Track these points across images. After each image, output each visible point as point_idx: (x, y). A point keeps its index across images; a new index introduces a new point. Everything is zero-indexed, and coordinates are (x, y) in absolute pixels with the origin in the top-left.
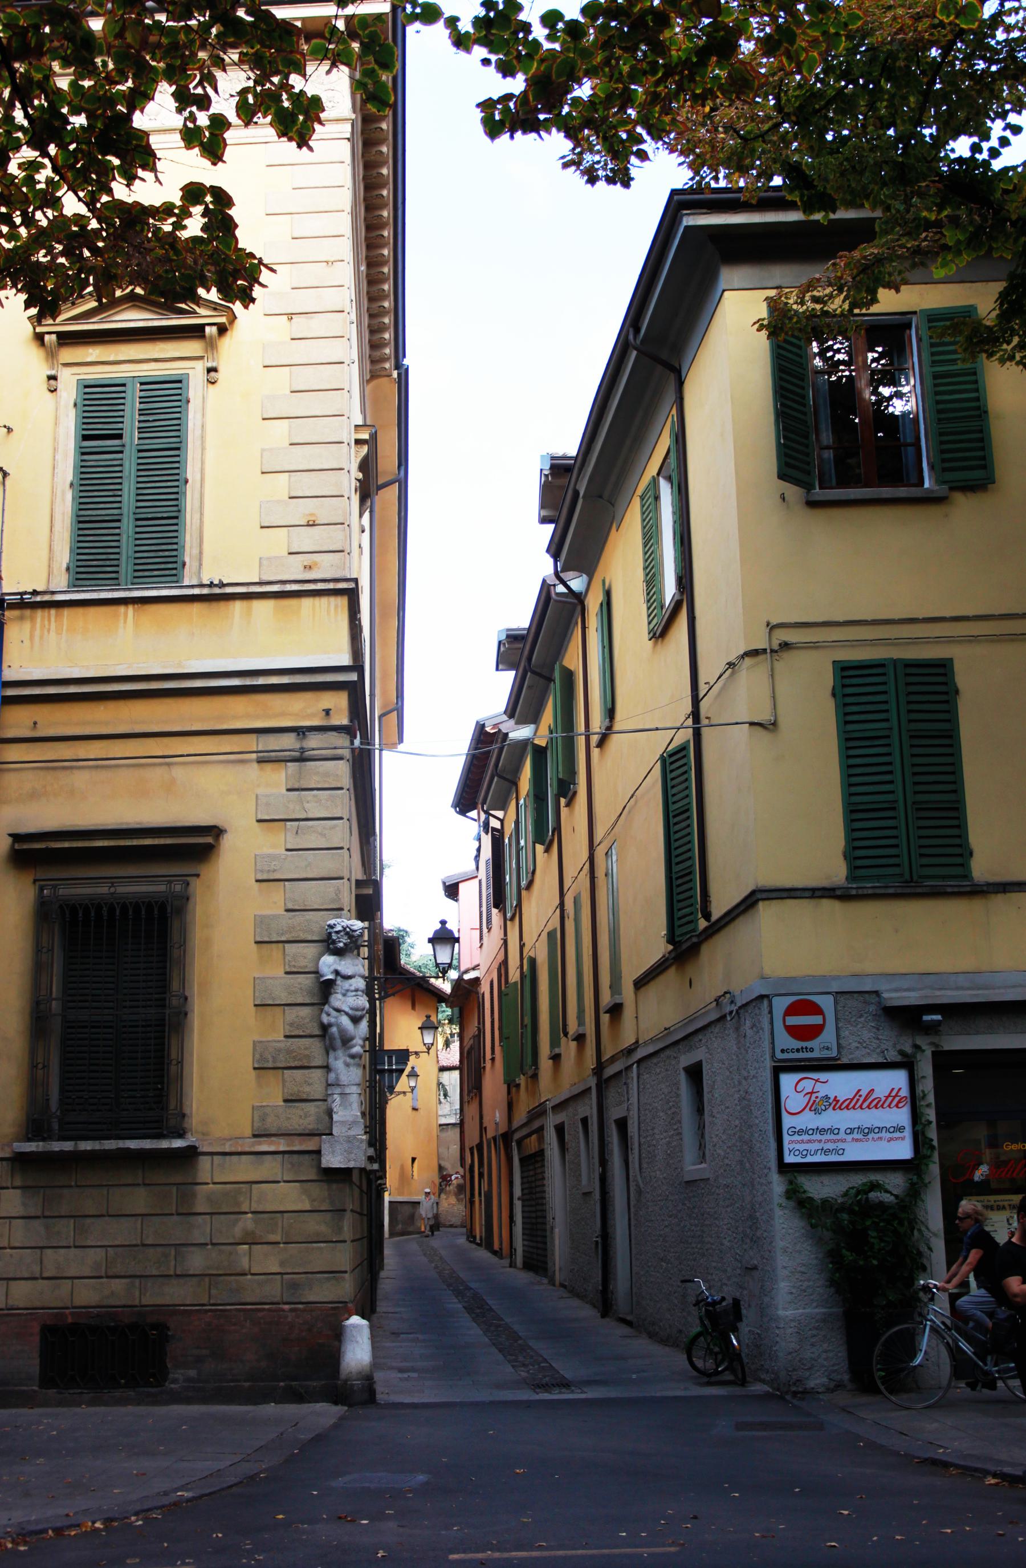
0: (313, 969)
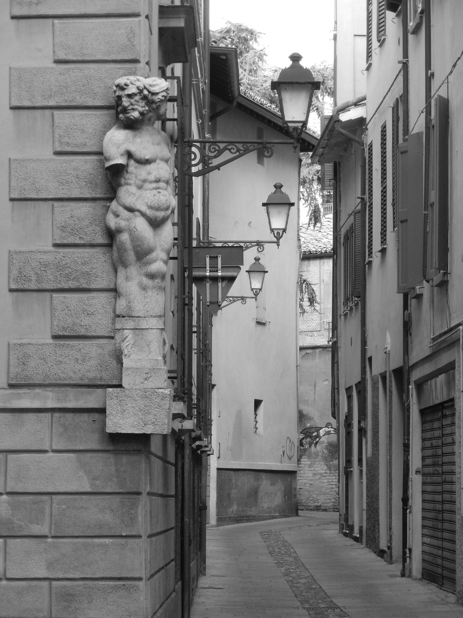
0: (94, 149)
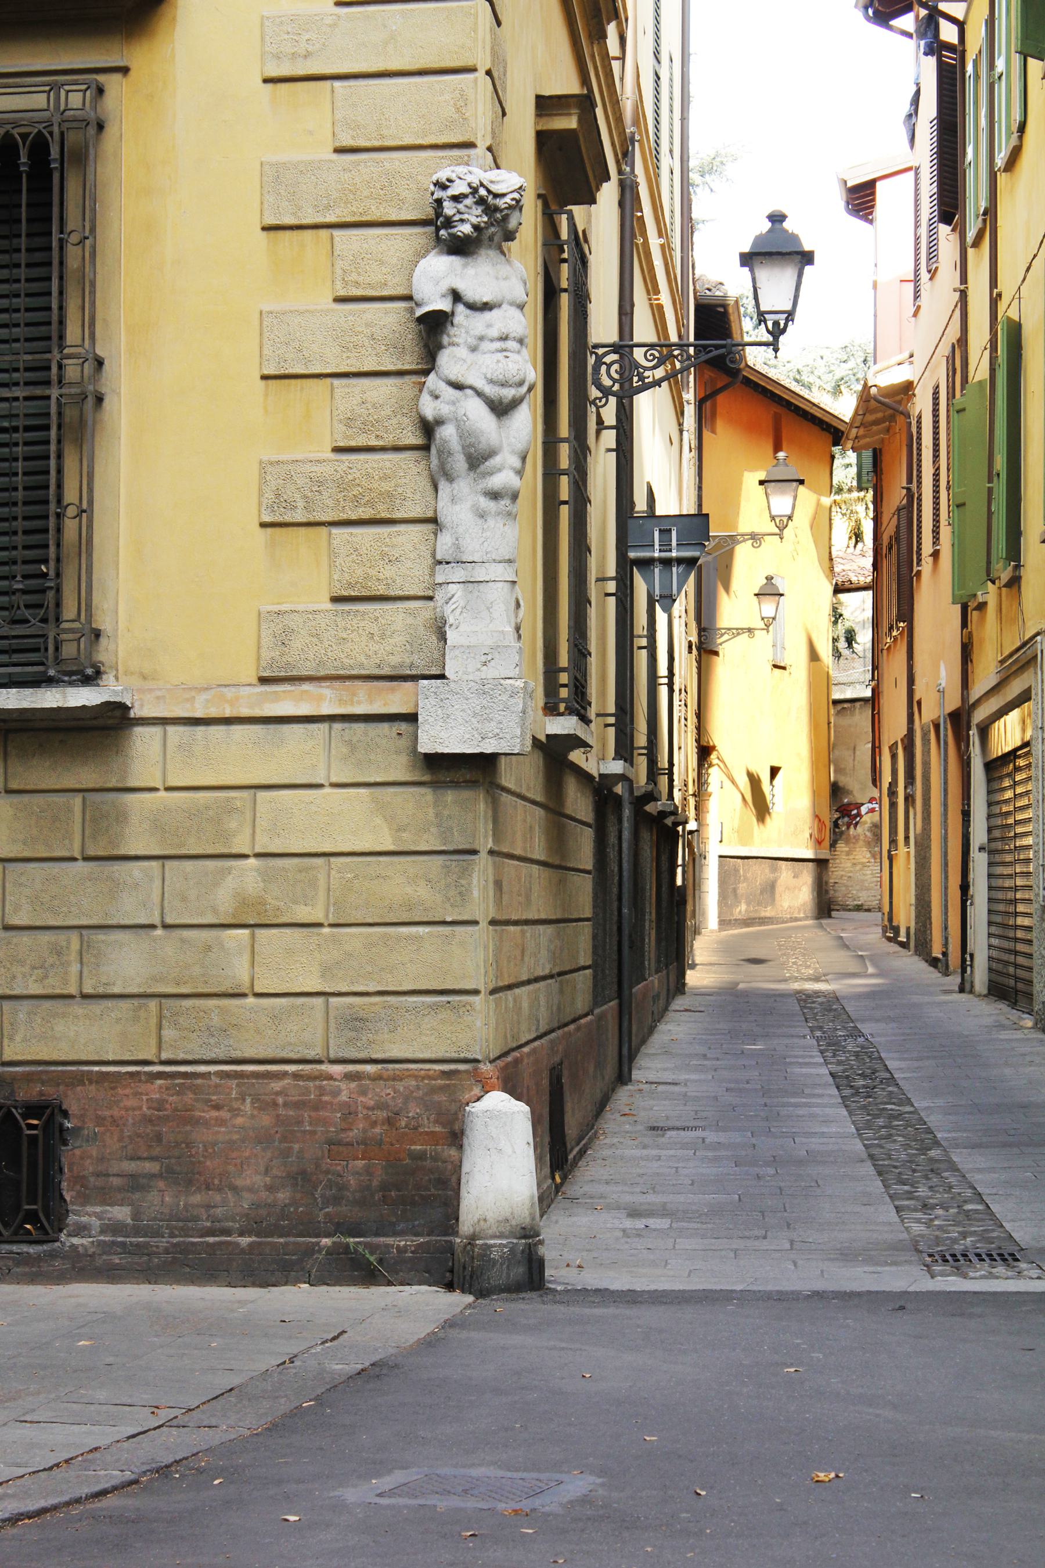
0: (401, 291)
